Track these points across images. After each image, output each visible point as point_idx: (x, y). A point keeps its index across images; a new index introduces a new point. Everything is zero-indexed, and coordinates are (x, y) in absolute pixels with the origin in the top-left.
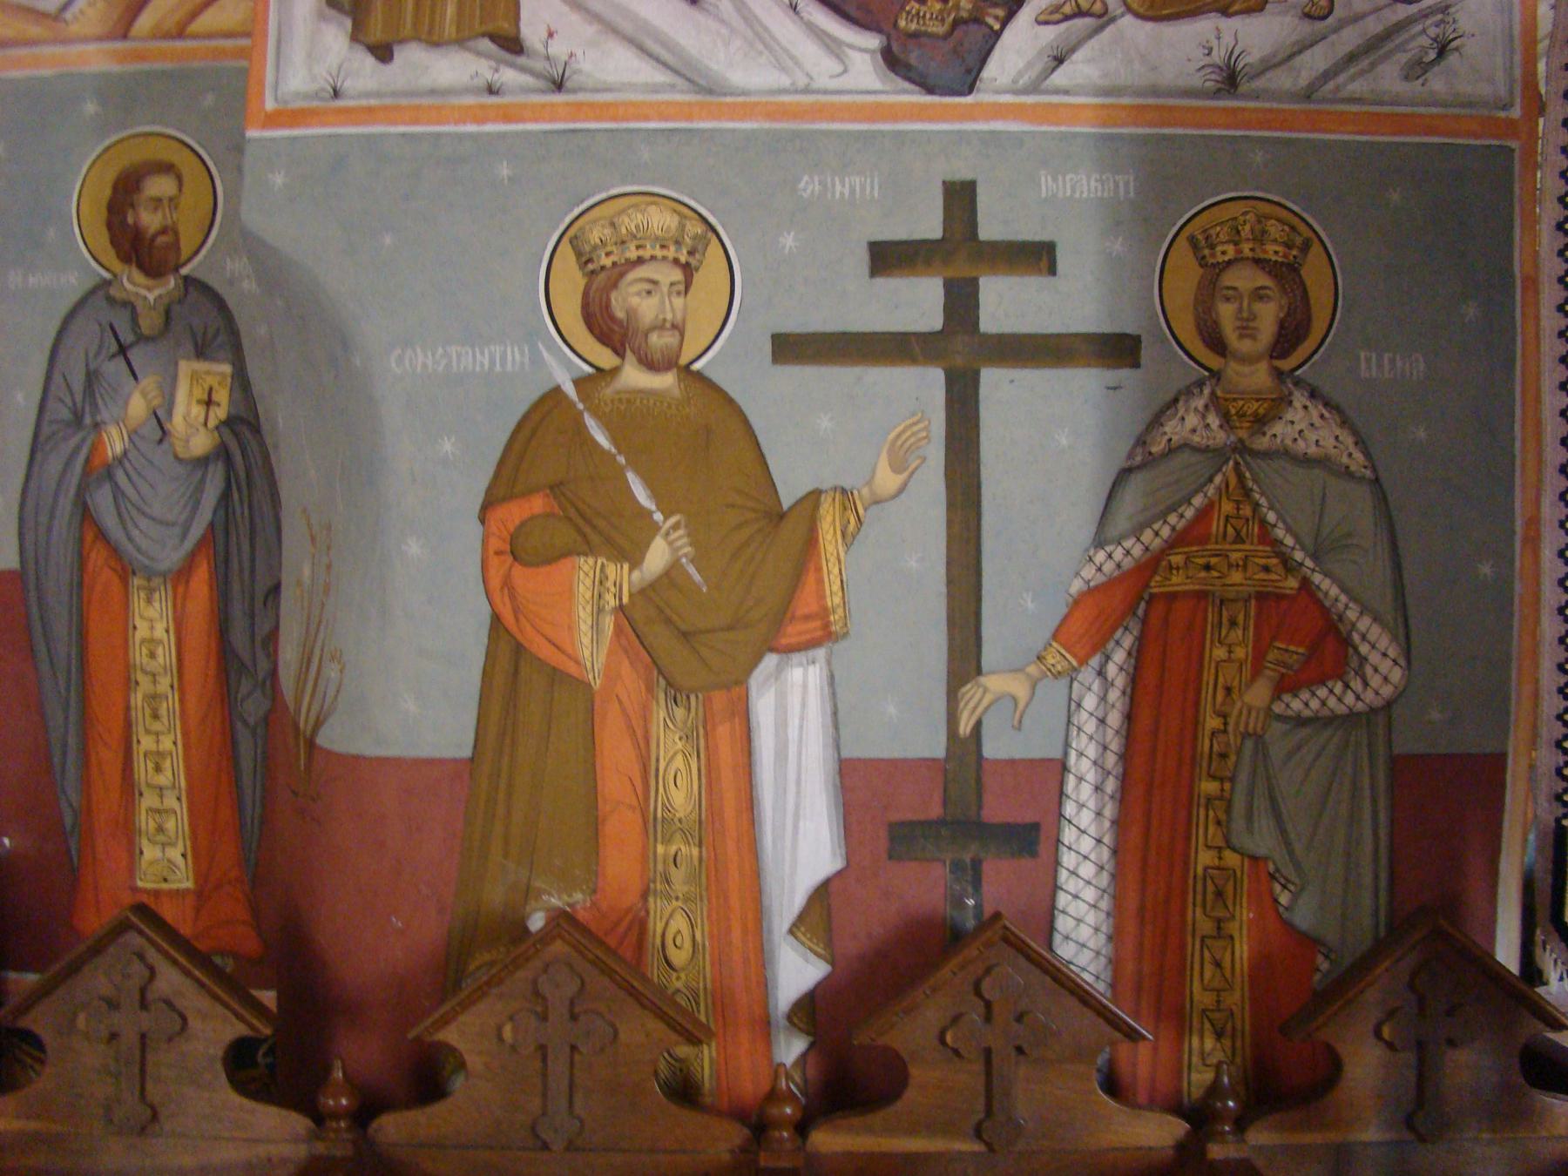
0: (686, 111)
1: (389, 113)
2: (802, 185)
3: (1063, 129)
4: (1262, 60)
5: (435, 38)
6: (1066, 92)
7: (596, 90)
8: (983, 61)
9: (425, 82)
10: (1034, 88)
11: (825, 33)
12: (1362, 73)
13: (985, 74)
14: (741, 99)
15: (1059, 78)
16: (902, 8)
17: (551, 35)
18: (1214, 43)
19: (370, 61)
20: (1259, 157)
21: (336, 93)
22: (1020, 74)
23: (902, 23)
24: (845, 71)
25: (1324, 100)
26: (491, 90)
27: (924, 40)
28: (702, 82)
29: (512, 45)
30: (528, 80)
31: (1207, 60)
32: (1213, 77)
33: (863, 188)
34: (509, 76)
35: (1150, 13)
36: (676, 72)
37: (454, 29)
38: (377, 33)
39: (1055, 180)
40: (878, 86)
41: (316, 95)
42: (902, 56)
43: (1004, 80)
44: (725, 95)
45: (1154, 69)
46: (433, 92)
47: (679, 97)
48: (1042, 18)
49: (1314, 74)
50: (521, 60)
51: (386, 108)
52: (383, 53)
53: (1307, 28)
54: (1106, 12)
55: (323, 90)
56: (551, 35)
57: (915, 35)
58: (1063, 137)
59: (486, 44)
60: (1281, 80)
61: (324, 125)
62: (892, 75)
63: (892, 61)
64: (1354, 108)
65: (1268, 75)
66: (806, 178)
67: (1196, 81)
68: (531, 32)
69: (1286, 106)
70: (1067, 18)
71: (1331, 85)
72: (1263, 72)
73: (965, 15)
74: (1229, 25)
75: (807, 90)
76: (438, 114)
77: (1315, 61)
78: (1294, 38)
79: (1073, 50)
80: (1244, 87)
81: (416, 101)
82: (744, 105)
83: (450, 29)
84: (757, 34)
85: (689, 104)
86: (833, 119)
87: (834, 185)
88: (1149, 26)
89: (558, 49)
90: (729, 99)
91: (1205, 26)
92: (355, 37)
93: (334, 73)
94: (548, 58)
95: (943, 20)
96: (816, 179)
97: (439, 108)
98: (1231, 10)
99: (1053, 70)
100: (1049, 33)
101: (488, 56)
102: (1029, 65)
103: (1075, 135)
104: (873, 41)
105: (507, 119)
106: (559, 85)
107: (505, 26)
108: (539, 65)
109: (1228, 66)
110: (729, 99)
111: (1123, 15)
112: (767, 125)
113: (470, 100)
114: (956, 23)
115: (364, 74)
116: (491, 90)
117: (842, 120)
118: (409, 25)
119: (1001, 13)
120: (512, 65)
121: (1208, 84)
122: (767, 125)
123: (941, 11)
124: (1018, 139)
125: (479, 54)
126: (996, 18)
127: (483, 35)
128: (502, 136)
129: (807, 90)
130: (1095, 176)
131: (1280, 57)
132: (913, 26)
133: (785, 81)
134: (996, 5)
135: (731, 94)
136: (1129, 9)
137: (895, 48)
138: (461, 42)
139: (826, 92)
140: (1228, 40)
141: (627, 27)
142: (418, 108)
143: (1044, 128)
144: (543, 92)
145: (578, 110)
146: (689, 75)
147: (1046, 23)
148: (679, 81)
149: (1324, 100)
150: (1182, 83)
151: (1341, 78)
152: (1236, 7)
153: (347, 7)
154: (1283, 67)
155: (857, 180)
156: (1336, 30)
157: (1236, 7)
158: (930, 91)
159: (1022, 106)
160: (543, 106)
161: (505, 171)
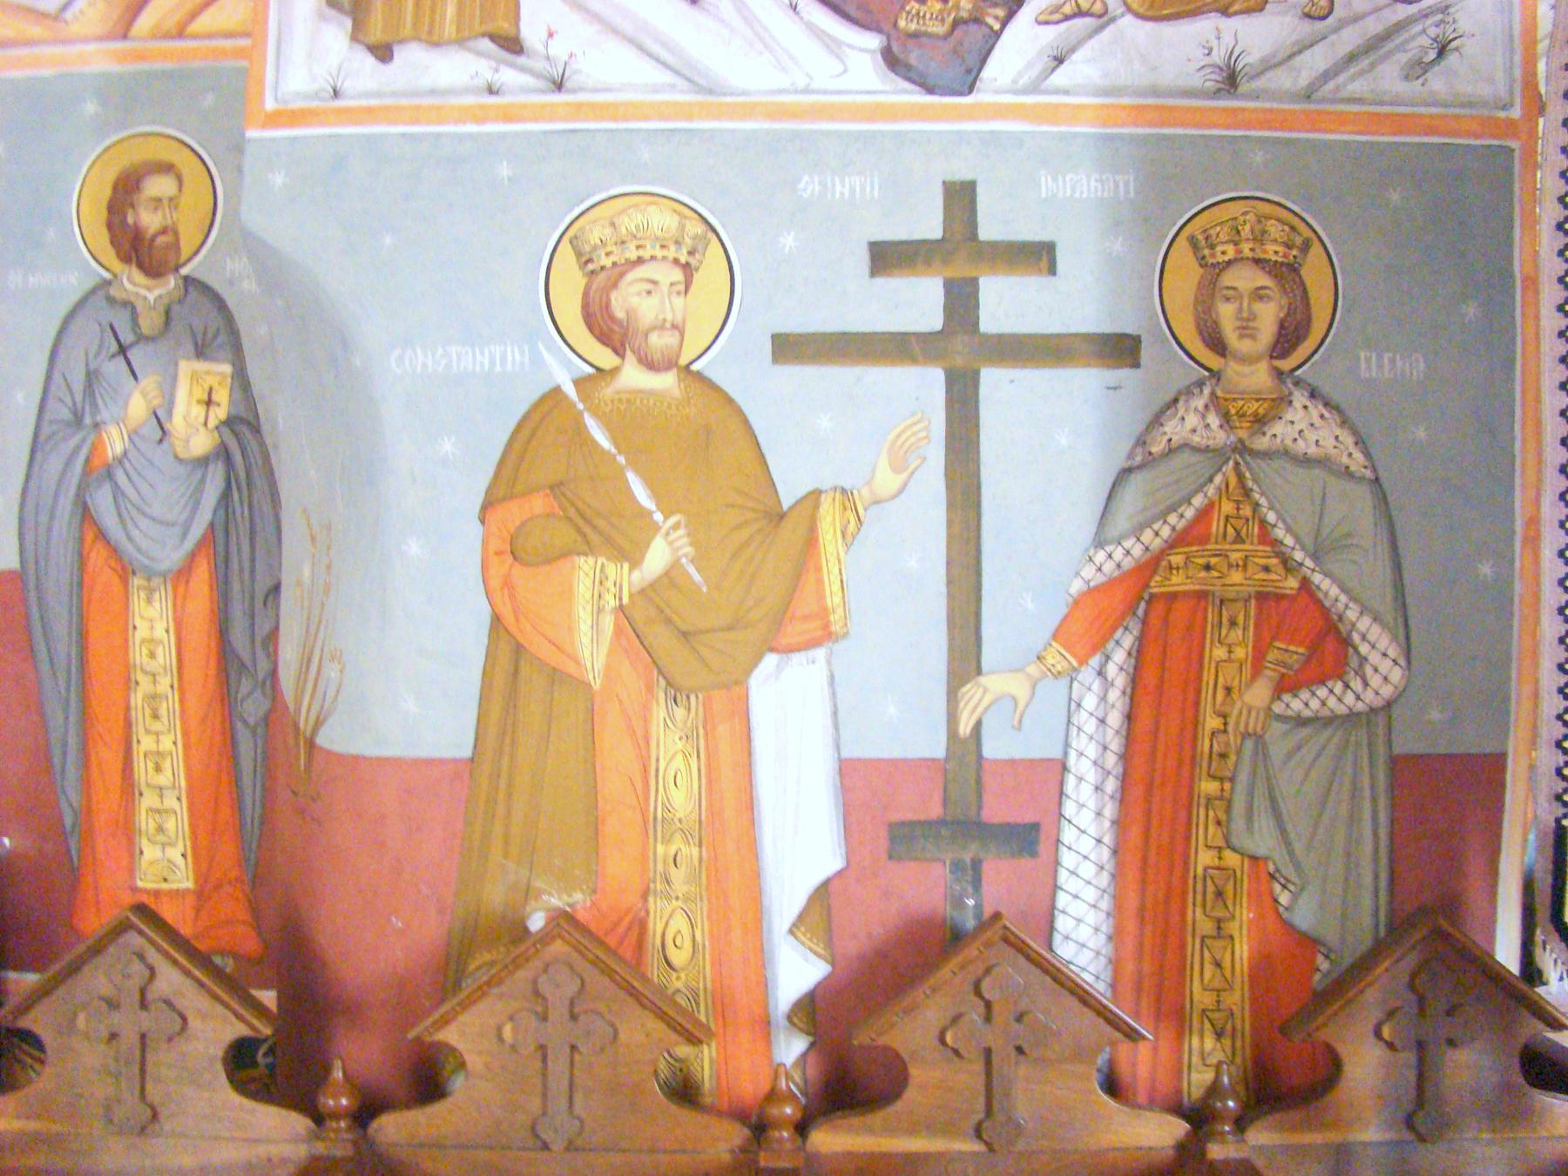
0: (685, 111)
1: (388, 114)
2: (801, 185)
3: (1063, 129)
4: (1263, 60)
5: (435, 38)
6: (1066, 92)
7: (596, 90)
8: (983, 61)
9: (426, 82)
10: (1034, 88)
11: (823, 32)
12: (1362, 73)
13: (988, 72)
14: (741, 99)
15: (1060, 78)
16: (903, 8)
17: (551, 35)
18: (1214, 43)
19: (370, 61)
20: (1259, 158)
21: (336, 93)
22: (1020, 74)
23: (902, 23)
24: (845, 71)
25: (1323, 100)
26: (491, 91)
27: (924, 40)
28: (702, 82)
29: (512, 45)
30: (528, 80)
31: (1207, 60)
32: (1213, 77)
33: (863, 189)
34: (509, 77)
35: (1149, 13)
36: (677, 73)
37: (454, 29)
38: (376, 34)
39: (1055, 180)
40: (879, 86)
41: (316, 95)
42: (902, 57)
43: (1004, 80)
44: (725, 94)
45: (1154, 69)
46: (432, 92)
47: (680, 98)
48: (1042, 18)
49: (1314, 74)
50: (522, 60)
51: (387, 109)
52: (383, 53)
53: (1308, 28)
54: (1106, 12)
55: (324, 90)
56: (551, 35)
57: (916, 35)
58: (1063, 137)
59: (486, 44)
60: (1282, 80)
61: (322, 124)
62: (892, 75)
63: (892, 61)
64: (1354, 108)
65: (1269, 75)
66: (806, 178)
67: (1197, 81)
68: (531, 33)
69: (1286, 106)
70: (1067, 18)
71: (1331, 85)
72: (1262, 72)
73: (965, 15)
74: (1229, 25)
75: (806, 91)
76: (439, 114)
77: (1316, 61)
78: (1295, 37)
79: (1073, 50)
80: (1243, 87)
81: (416, 101)
82: (744, 105)
83: (450, 29)
84: (757, 34)
85: (690, 105)
86: (832, 119)
87: (834, 186)
88: (1149, 26)
89: (558, 49)
90: (729, 99)
91: (1205, 26)
92: (354, 38)
93: (334, 73)
94: (548, 58)
95: (943, 21)
96: (816, 179)
97: (439, 108)
98: (1231, 10)
99: (1053, 70)
100: (1050, 34)
101: (488, 56)
102: (1030, 65)
103: (1075, 136)
104: (873, 41)
105: (508, 119)
106: (559, 86)
107: (503, 26)
108: (539, 65)
109: (1228, 65)
110: (729, 99)
111: (1123, 15)
112: (766, 125)
113: (470, 100)
114: (956, 24)
115: (364, 74)
116: (491, 91)
117: (843, 120)
118: (409, 25)
119: (1001, 13)
120: (512, 65)
121: (1208, 84)
122: (766, 125)
123: (941, 11)
124: (1017, 140)
125: (479, 54)
126: (996, 18)
127: (483, 35)
128: (502, 136)
129: (806, 91)
130: (1095, 176)
131: (1280, 57)
132: (913, 27)
133: (783, 82)
134: (996, 5)
135: (732, 94)
136: (1129, 9)
137: (895, 48)
138: (461, 41)
139: (825, 92)
140: (1228, 40)
141: (627, 27)
142: (418, 108)
143: (1045, 128)
144: (543, 92)
145: (579, 110)
146: (688, 74)
147: (1047, 23)
148: (680, 82)
149: (1323, 100)
150: (1183, 82)
151: (1341, 79)
152: (1236, 7)
153: (347, 6)
154: (1284, 67)
155: (857, 180)
156: (1336, 30)
157: (1236, 7)
158: (930, 91)
159: (1022, 106)
160: (543, 106)
161: (504, 170)
